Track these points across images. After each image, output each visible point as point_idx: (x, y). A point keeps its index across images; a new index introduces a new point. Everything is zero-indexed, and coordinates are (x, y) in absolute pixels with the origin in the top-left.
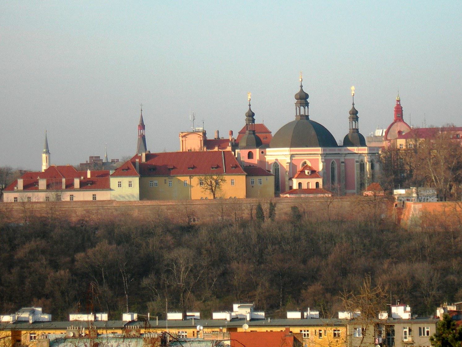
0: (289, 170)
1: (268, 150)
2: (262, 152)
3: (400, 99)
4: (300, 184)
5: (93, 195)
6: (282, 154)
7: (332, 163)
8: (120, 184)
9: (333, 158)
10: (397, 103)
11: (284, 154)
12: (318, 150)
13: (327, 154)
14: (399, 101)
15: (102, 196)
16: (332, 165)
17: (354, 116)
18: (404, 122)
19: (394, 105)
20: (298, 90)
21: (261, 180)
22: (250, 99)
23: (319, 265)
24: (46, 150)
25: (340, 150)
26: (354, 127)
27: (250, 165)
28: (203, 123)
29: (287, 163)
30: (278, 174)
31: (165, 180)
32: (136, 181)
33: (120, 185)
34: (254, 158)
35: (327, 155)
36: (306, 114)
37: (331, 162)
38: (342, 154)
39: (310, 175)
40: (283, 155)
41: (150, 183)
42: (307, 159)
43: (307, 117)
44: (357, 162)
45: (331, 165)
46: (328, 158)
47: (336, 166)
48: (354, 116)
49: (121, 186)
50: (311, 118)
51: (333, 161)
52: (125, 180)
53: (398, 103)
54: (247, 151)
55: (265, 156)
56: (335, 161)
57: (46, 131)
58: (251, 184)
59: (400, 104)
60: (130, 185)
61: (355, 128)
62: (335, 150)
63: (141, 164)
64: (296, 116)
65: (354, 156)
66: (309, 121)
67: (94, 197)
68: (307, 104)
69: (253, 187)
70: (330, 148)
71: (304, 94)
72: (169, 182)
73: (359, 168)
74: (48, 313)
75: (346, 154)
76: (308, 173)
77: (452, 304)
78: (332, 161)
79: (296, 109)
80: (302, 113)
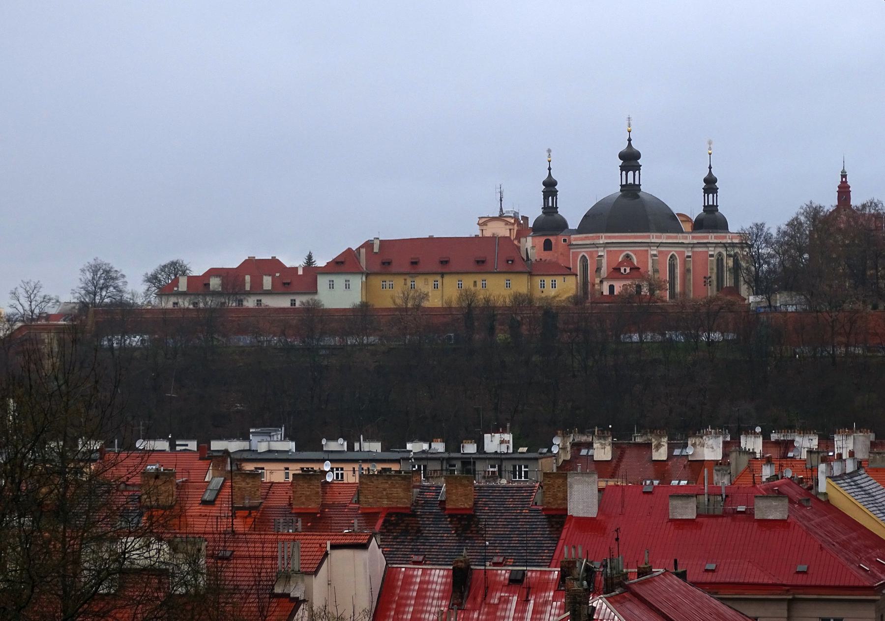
4: (612, 288)
7: (671, 257)
9: (673, 251)
10: (842, 179)
14: (844, 176)
15: (742, 283)
17: (710, 185)
19: (838, 180)
20: (624, 147)
25: (686, 238)
26: (711, 203)
31: (405, 280)
34: (546, 252)
36: (637, 183)
37: (669, 256)
41: (383, 285)
42: (584, 252)
44: (712, 256)
47: (678, 261)
48: (710, 185)
49: (333, 288)
51: (673, 255)
54: (543, 239)
56: (675, 254)
59: (846, 182)
60: (347, 287)
65: (708, 247)
67: (293, 303)
68: (637, 168)
69: (542, 292)
74: (292, 440)
77: (812, 432)
79: (621, 175)
80: (630, 181)
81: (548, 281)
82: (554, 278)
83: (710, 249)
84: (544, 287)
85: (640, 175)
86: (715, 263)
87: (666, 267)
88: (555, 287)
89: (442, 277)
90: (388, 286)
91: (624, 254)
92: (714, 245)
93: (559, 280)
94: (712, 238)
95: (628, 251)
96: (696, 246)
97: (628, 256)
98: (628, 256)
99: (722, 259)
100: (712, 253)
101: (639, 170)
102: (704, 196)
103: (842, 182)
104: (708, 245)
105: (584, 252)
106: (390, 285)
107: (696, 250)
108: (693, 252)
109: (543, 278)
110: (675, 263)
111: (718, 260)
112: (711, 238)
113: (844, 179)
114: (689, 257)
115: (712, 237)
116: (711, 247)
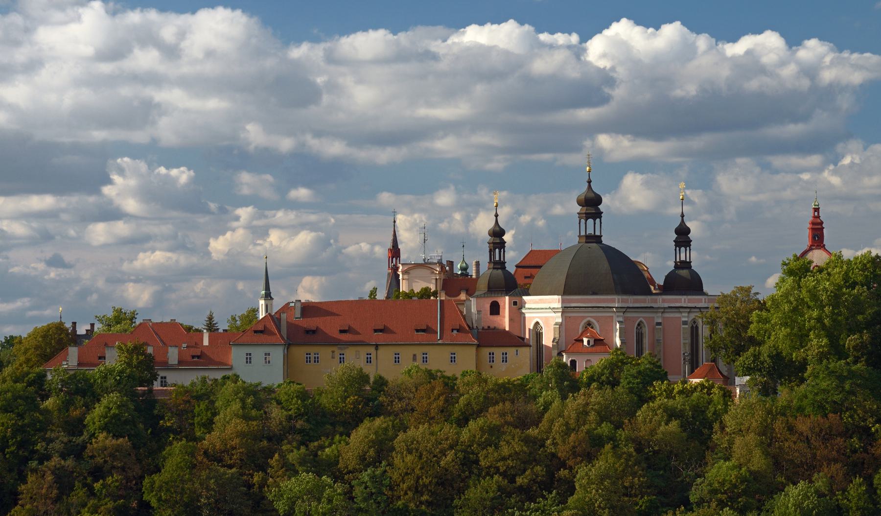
0: (558, 336)
1: (530, 301)
2: (515, 303)
3: (818, 206)
5: (247, 354)
6: (548, 307)
7: (639, 325)
8: (250, 358)
9: (641, 316)
11: (551, 307)
12: (613, 301)
13: (628, 308)
14: (817, 210)
16: (639, 328)
17: (683, 237)
18: (825, 249)
21: (506, 354)
22: (497, 203)
23: (83, 459)
24: (265, 293)
25: (655, 301)
27: (489, 327)
28: (463, 246)
29: (556, 324)
30: (640, 348)
31: (333, 352)
32: (277, 354)
33: (249, 360)
35: (628, 310)
36: (598, 233)
38: (659, 308)
39: (592, 346)
40: (550, 308)
42: (591, 317)
43: (597, 239)
44: (685, 323)
45: (637, 328)
46: (628, 315)
47: (646, 330)
49: (250, 362)
50: (605, 241)
51: (641, 321)
52: (258, 353)
53: (816, 214)
55: (523, 311)
56: (643, 320)
57: (266, 258)
58: (488, 361)
59: (818, 217)
61: (684, 259)
62: (680, 301)
63: (290, 325)
64: (580, 236)
65: (681, 312)
66: (601, 245)
68: (598, 215)
69: (491, 367)
70: (690, 297)
71: (593, 195)
72: (306, 356)
73: (688, 335)
75: (665, 308)
76: (589, 342)
78: (639, 320)
80: (590, 231)
81: (498, 352)
82: (504, 350)
83: (683, 314)
84: (493, 361)
85: (601, 223)
86: (689, 330)
87: (634, 336)
88: (506, 362)
89: (377, 349)
90: (312, 360)
91: (585, 321)
92: (688, 310)
93: (511, 351)
94: (683, 300)
95: (589, 317)
96: (666, 310)
97: (589, 324)
98: (589, 324)
99: (697, 327)
100: (686, 319)
101: (600, 217)
102: (676, 250)
103: (815, 217)
104: (681, 310)
105: (591, 317)
106: (315, 357)
107: (667, 315)
108: (664, 318)
109: (492, 350)
110: (643, 332)
111: (692, 327)
112: (685, 302)
113: (816, 214)
114: (659, 324)
115: (685, 299)
116: (684, 312)
